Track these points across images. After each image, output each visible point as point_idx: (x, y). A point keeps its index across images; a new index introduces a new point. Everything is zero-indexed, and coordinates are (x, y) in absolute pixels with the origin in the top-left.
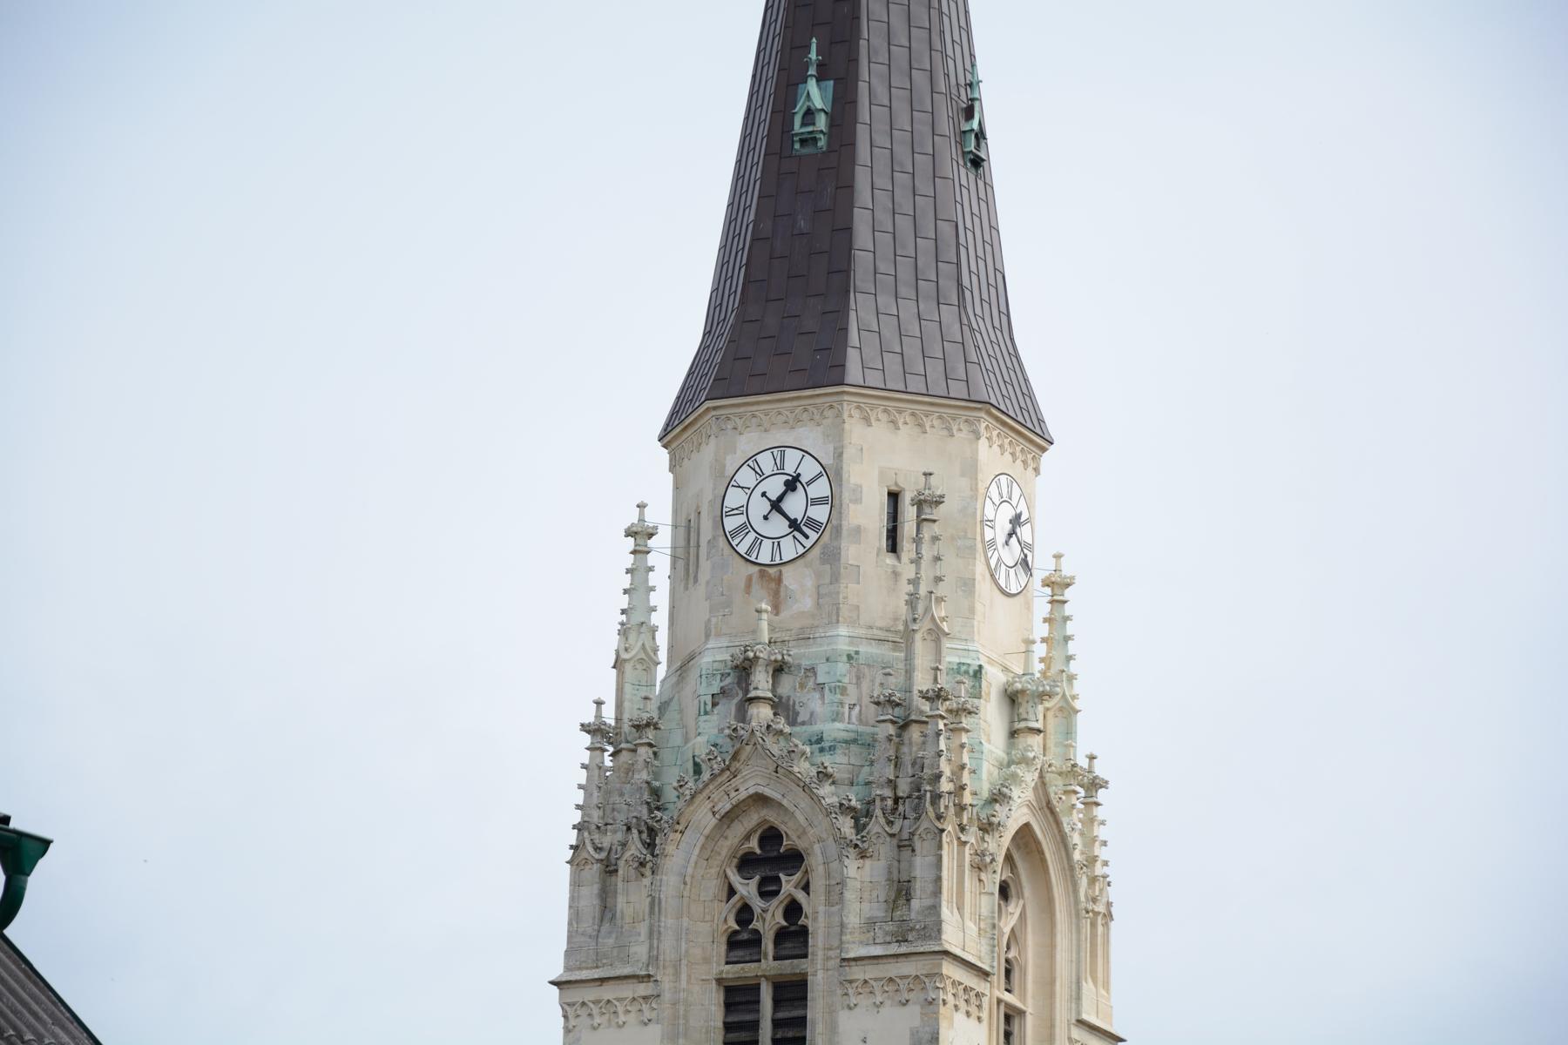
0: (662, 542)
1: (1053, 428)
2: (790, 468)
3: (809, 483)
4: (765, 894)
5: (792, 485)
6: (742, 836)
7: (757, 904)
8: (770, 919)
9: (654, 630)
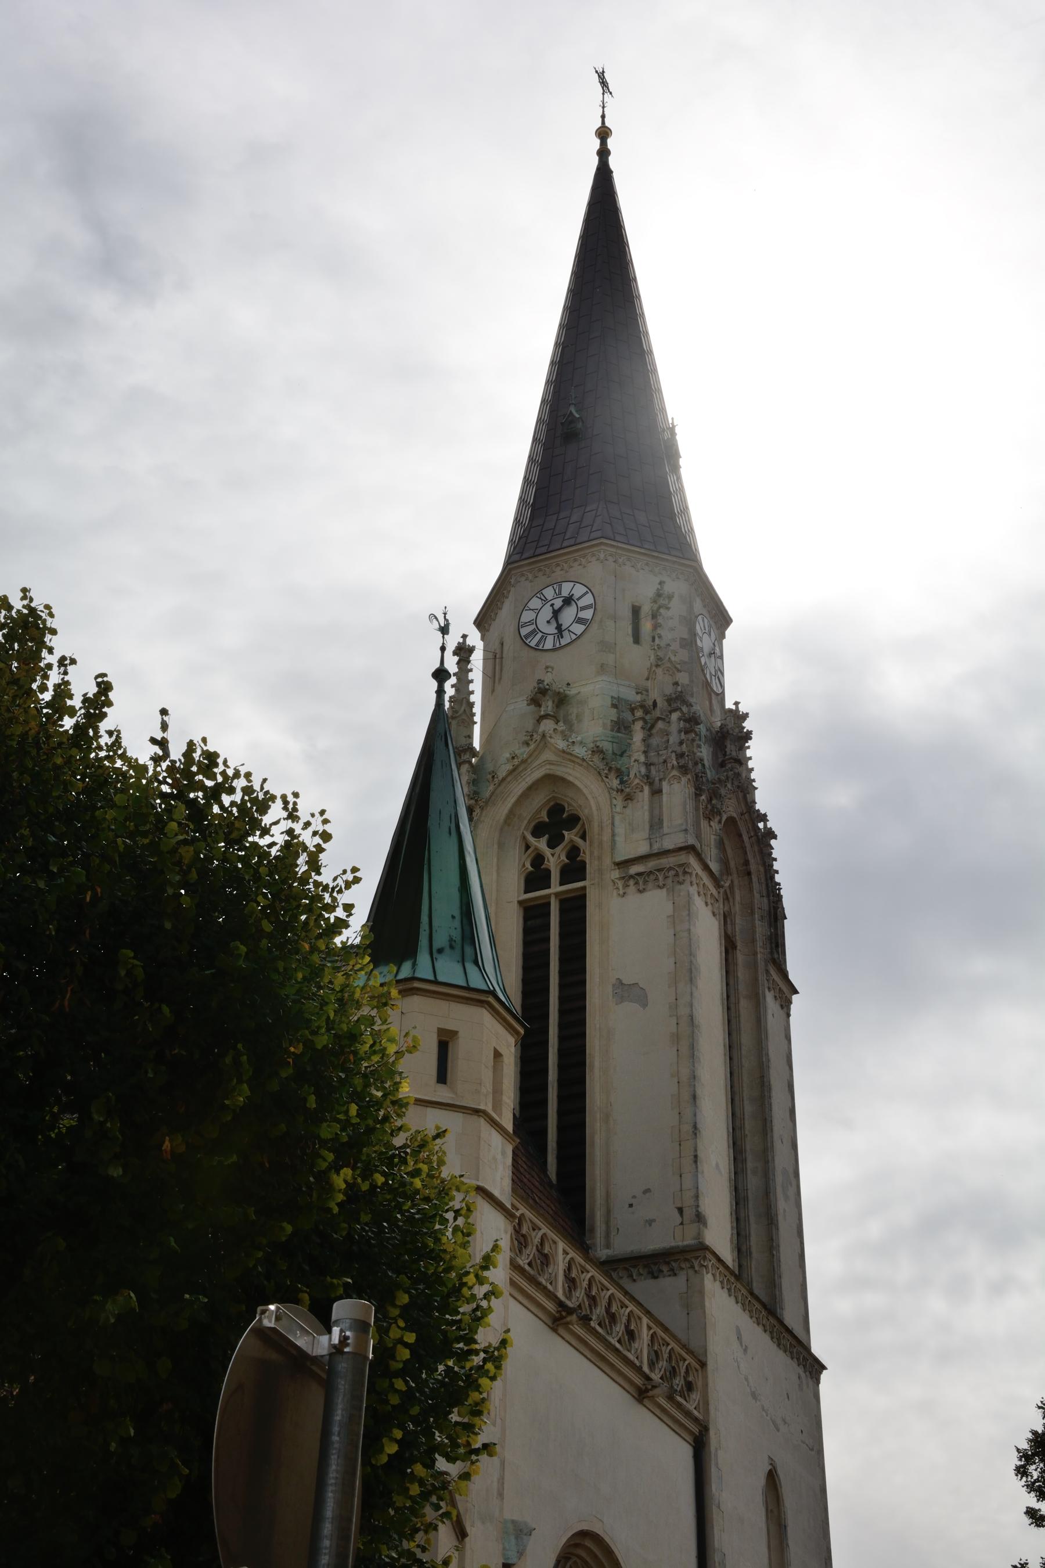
0: (477, 660)
1: (732, 613)
2: (565, 593)
3: (578, 599)
4: (552, 845)
5: (568, 601)
6: (537, 807)
7: (547, 852)
8: (555, 860)
9: (472, 705)
